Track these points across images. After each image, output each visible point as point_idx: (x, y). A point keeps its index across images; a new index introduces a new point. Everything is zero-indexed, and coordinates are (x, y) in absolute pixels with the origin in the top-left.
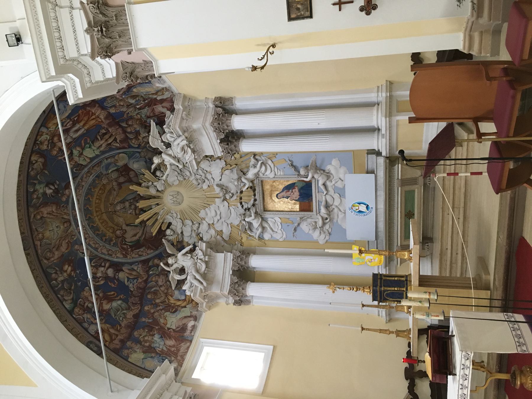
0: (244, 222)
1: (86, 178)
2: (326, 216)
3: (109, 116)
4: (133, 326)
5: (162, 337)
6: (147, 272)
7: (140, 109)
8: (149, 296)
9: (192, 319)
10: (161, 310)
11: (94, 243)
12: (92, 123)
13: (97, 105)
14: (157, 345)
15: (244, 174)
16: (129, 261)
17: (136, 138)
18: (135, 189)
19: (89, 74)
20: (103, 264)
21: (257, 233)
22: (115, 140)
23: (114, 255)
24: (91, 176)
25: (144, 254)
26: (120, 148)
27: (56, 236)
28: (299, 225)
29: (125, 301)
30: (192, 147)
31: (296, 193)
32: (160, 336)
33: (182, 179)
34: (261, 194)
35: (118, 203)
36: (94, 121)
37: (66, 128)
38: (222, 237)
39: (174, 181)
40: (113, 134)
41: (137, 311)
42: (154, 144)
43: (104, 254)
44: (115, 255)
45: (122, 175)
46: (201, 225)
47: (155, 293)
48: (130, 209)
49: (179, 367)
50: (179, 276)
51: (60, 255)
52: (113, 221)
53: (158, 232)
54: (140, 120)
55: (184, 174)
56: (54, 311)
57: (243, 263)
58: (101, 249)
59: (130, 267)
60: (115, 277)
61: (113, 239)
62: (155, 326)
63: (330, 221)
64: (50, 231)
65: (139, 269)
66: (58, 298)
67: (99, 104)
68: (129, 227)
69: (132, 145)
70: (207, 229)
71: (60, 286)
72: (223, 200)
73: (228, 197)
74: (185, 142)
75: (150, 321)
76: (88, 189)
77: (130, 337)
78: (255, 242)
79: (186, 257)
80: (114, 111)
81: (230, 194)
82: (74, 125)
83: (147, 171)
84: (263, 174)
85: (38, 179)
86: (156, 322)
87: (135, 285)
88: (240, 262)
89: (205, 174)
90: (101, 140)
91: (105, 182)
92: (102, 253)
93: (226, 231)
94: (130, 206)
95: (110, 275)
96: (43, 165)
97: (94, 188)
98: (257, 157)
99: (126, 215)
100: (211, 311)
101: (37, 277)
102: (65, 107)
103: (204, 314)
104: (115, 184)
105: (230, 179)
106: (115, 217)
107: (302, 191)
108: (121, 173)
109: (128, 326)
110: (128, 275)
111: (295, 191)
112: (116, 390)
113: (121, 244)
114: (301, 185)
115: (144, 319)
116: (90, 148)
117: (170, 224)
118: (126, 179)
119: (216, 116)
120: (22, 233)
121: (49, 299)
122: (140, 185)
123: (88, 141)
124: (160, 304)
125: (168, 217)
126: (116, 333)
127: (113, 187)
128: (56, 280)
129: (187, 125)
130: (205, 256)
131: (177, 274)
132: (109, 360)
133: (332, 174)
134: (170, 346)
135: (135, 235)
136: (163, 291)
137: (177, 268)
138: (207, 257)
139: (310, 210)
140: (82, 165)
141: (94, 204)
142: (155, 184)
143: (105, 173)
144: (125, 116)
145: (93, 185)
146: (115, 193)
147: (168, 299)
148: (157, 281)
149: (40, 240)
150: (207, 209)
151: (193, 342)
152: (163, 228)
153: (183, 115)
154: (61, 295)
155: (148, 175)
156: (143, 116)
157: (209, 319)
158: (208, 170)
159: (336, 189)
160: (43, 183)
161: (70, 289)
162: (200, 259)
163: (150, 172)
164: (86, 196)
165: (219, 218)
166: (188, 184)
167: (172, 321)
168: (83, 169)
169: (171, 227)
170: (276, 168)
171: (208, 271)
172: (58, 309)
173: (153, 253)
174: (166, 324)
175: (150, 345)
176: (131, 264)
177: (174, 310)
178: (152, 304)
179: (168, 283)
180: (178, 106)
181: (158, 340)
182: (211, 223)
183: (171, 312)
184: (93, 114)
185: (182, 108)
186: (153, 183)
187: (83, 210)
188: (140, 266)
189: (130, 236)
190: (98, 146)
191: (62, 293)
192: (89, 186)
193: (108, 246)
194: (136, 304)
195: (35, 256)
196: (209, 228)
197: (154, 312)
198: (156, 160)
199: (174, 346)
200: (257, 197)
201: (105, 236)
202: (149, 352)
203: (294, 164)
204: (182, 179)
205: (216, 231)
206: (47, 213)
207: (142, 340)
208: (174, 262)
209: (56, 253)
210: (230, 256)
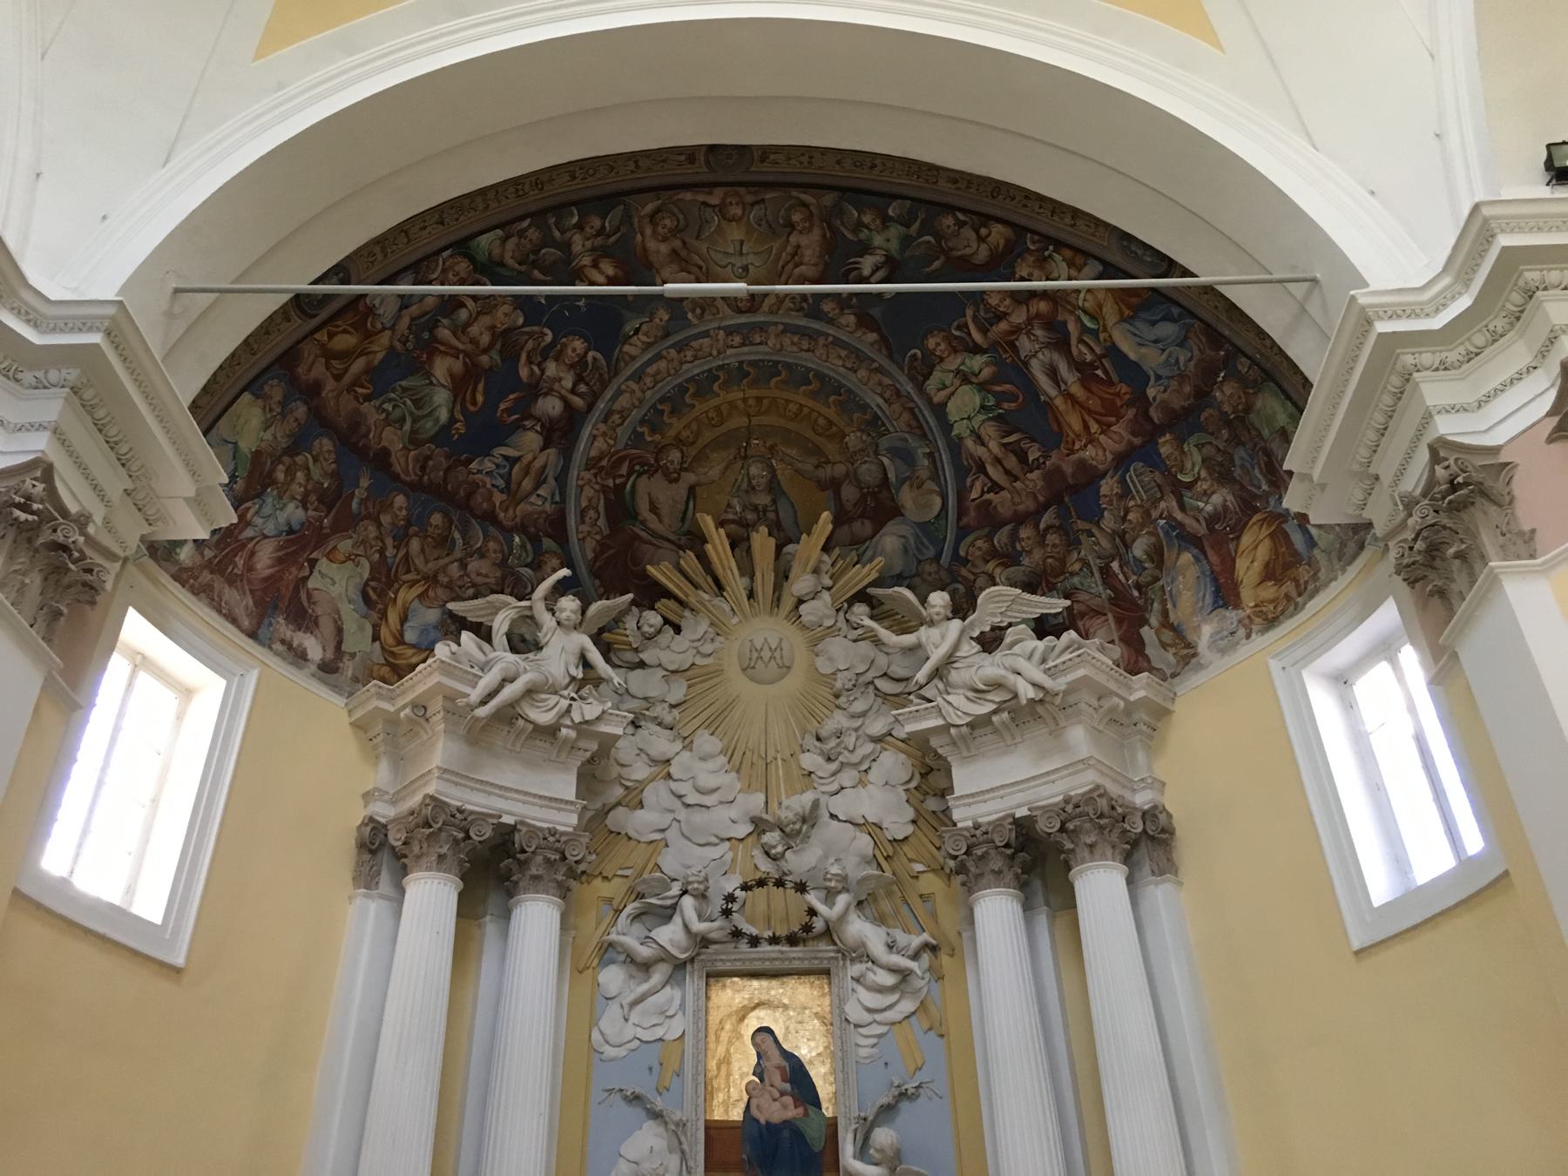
0: (676, 889)
1: (880, 384)
3: (1090, 476)
4: (354, 445)
5: (291, 531)
6: (522, 529)
7: (1106, 572)
8: (437, 519)
9: (330, 655)
10: (382, 552)
11: (658, 372)
12: (1074, 421)
13: (1137, 441)
14: (267, 510)
15: (860, 903)
16: (574, 473)
17: (993, 554)
18: (817, 529)
19: (1444, 367)
20: (582, 388)
21: (629, 937)
22: (996, 487)
23: (602, 427)
24: (880, 401)
25: (585, 528)
26: (961, 498)
28: (657, 1115)
29: (442, 436)
30: (995, 719)
32: (296, 527)
34: (777, 965)
37: (1074, 341)
38: (619, 804)
39: (830, 659)
40: (1018, 484)
41: (398, 469)
42: (990, 598)
43: (614, 398)
44: (604, 434)
45: (863, 497)
46: (668, 732)
47: (444, 542)
48: (744, 508)
49: (174, 569)
50: (505, 628)
53: (657, 584)
54: (1062, 570)
55: (857, 693)
56: (482, 192)
57: (534, 871)
59: (551, 473)
60: (531, 416)
61: (657, 437)
62: (334, 513)
64: (742, 243)
65: (539, 503)
67: (1142, 446)
68: (684, 493)
69: (969, 539)
70: (653, 753)
71: (557, 234)
72: (756, 821)
73: (772, 837)
74: (1027, 692)
75: (354, 505)
76: (841, 385)
77: (320, 421)
78: (591, 932)
79: (573, 660)
80: (1104, 490)
81: (780, 849)
82: (1078, 365)
83: (874, 575)
84: (857, 980)
85: (920, 234)
86: (346, 523)
87: (488, 480)
88: (539, 859)
89: (855, 765)
90: (1004, 445)
91: (853, 439)
92: (619, 393)
93: (641, 822)
94: (755, 508)
95: (540, 402)
96: (962, 259)
98: (926, 957)
100: (348, 730)
102: (1156, 342)
103: (340, 701)
104: (840, 470)
105: (836, 851)
107: (786, 1134)
109: (356, 422)
110: (525, 461)
111: (785, 1107)
112: (177, 309)
116: (983, 407)
117: (678, 630)
118: (848, 506)
120: (766, 152)
123: (1006, 405)
124: (402, 553)
125: (704, 626)
126: (347, 379)
127: (828, 462)
128: (580, 227)
129: (1083, 706)
134: (252, 554)
135: (654, 509)
136: (445, 567)
137: (538, 626)
138: (573, 734)
140: (927, 377)
142: (826, 596)
143: (884, 443)
144: (1081, 525)
145: (850, 402)
146: (809, 467)
147: (413, 584)
149: (721, 209)
150: (723, 759)
151: (251, 641)
152: (662, 604)
153: (1116, 700)
154: (526, 230)
155: (862, 575)
156: (1076, 580)
157: (325, 713)
158: (872, 776)
161: (534, 264)
162: (568, 710)
163: (871, 585)
165: (689, 800)
166: (765, 712)
167: (335, 582)
168: (912, 379)
169: (670, 631)
170: (883, 1029)
171: (523, 731)
172: (487, 207)
173: (584, 555)
174: (330, 557)
175: (273, 482)
176: (562, 479)
177: (374, 597)
178: (409, 524)
179: (471, 592)
180: (1141, 687)
181: (282, 517)
182: (674, 770)
183: (366, 584)
184: (1106, 428)
185: (1132, 698)
186: (829, 589)
187: (775, 358)
188: (548, 507)
189: (657, 496)
190: (982, 432)
191: (533, 234)
192: (849, 391)
193: (636, 414)
194: (423, 468)
196: (654, 762)
197: (379, 525)
198: (939, 599)
199: (250, 568)
200: (765, 948)
201: (672, 412)
203: (905, 1105)
204: (839, 685)
206: (798, 247)
207: (299, 459)
208: (564, 615)
209: (664, 248)
210: (567, 821)
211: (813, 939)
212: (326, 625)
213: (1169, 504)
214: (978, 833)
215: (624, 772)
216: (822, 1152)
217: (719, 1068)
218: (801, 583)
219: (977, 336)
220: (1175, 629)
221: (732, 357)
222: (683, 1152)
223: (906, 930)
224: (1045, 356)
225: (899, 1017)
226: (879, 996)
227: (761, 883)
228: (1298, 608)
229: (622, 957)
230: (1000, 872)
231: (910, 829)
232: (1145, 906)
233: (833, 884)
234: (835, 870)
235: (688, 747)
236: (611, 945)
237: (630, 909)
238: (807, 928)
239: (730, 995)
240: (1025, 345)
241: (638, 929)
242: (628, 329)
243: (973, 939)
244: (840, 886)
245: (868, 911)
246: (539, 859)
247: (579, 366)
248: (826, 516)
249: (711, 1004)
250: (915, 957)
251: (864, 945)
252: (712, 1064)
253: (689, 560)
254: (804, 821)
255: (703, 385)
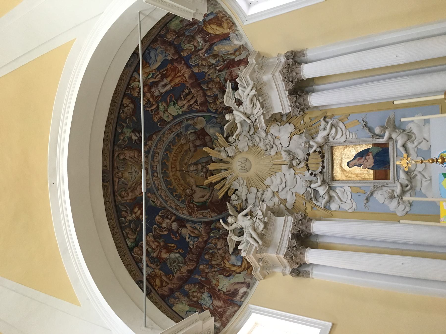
0: (309, 189)
1: (167, 134)
2: (407, 182)
3: (193, 75)
5: (211, 296)
6: (209, 233)
7: (220, 71)
8: (206, 257)
9: (245, 285)
10: (216, 272)
11: (165, 196)
12: (178, 80)
14: (205, 303)
16: (193, 219)
17: (214, 102)
18: (208, 151)
20: (169, 217)
21: (322, 202)
22: (196, 102)
23: (180, 211)
24: (172, 134)
25: (208, 216)
26: (199, 111)
27: (133, 179)
28: (372, 194)
29: (183, 255)
30: (261, 101)
31: (370, 160)
32: (209, 295)
33: (251, 145)
34: (330, 161)
35: (192, 164)
36: (179, 79)
37: (155, 80)
38: (285, 205)
39: (244, 147)
40: (195, 95)
41: (193, 268)
42: (227, 103)
45: (199, 139)
47: (213, 255)
49: (222, 327)
50: (237, 237)
51: (133, 197)
52: (185, 180)
53: (224, 196)
54: (219, 83)
55: (254, 140)
56: (116, 244)
57: (305, 228)
58: (170, 203)
59: (193, 226)
61: (183, 196)
63: (411, 188)
64: (129, 173)
65: (201, 229)
66: (123, 233)
67: (185, 61)
68: (198, 188)
71: (127, 224)
73: (294, 163)
75: (203, 279)
76: (168, 145)
77: (180, 288)
79: (245, 218)
80: (197, 71)
81: (297, 161)
82: (162, 79)
83: (221, 135)
85: (126, 123)
86: (208, 282)
88: (301, 227)
90: (184, 99)
91: (183, 142)
92: (171, 207)
93: (290, 200)
94: (202, 169)
95: (173, 228)
97: (173, 145)
98: (327, 120)
99: (197, 176)
100: (266, 280)
101: (109, 208)
102: (156, 57)
103: (258, 282)
104: (191, 145)
105: (298, 145)
106: (187, 175)
107: (377, 158)
108: (198, 136)
109: (180, 279)
110: (190, 233)
111: (369, 158)
113: (189, 203)
114: (376, 150)
115: (197, 276)
116: (174, 105)
117: (236, 190)
118: (201, 143)
119: (286, 66)
120: (104, 166)
121: (114, 232)
122: (213, 149)
123: (173, 99)
125: (235, 183)
126: (168, 281)
128: (125, 217)
130: (264, 217)
131: (235, 235)
132: (148, 294)
133: (414, 134)
134: (217, 306)
135: (203, 197)
139: (386, 177)
140: (165, 121)
141: (171, 160)
142: (226, 149)
144: (206, 78)
145: (172, 143)
146: (191, 154)
147: (224, 263)
148: (217, 244)
149: (120, 178)
150: (273, 177)
151: (241, 307)
153: (256, 67)
154: (126, 232)
155: (221, 139)
156: (222, 79)
157: (261, 286)
158: (277, 135)
159: (419, 152)
160: (130, 128)
161: (136, 230)
162: (260, 219)
164: (165, 151)
165: (284, 186)
166: (259, 165)
168: (166, 125)
169: (237, 192)
170: (347, 131)
175: (197, 301)
176: (195, 223)
177: (228, 274)
178: (208, 264)
179: (226, 247)
180: (252, 60)
181: (207, 299)
183: (225, 276)
185: (255, 63)
186: (225, 148)
187: (160, 163)
188: (203, 226)
189: (199, 196)
191: (127, 230)
192: (169, 142)
193: (176, 202)
194: (193, 261)
195: (112, 190)
196: (273, 196)
197: (208, 272)
199: (221, 307)
200: (325, 164)
202: (195, 307)
203: (369, 125)
204: (251, 145)
205: (280, 199)
206: (130, 157)
207: (191, 294)
208: (233, 221)
209: (130, 194)
210: (290, 219)
211: (322, 151)
212: (236, 287)
213: (201, 53)
214: (293, 105)
215: (276, 204)
216: (382, 148)
217: (359, 177)
218: (223, 156)
219: (154, 107)
220: (236, 51)
221: (160, 175)
222: (382, 186)
223: (320, 125)
224: (160, 88)
225: (344, 127)
226: (338, 133)
227: (307, 165)
228: (230, 17)
229: (328, 204)
230: (304, 99)
231: (292, 124)
232: (313, 59)
233: (307, 146)
234: (303, 145)
235: (269, 187)
236: (325, 207)
237: (314, 202)
238: (319, 153)
239: (338, 174)
240: (157, 94)
241: (320, 200)
242: (153, 204)
243: (322, 106)
244: (308, 144)
245: (314, 136)
246: (301, 227)
247: (164, 218)
248: (204, 149)
249: (341, 179)
250: (327, 123)
251: (324, 137)
252: (357, 178)
253: (217, 187)
254: (290, 154)
255: (168, 183)
